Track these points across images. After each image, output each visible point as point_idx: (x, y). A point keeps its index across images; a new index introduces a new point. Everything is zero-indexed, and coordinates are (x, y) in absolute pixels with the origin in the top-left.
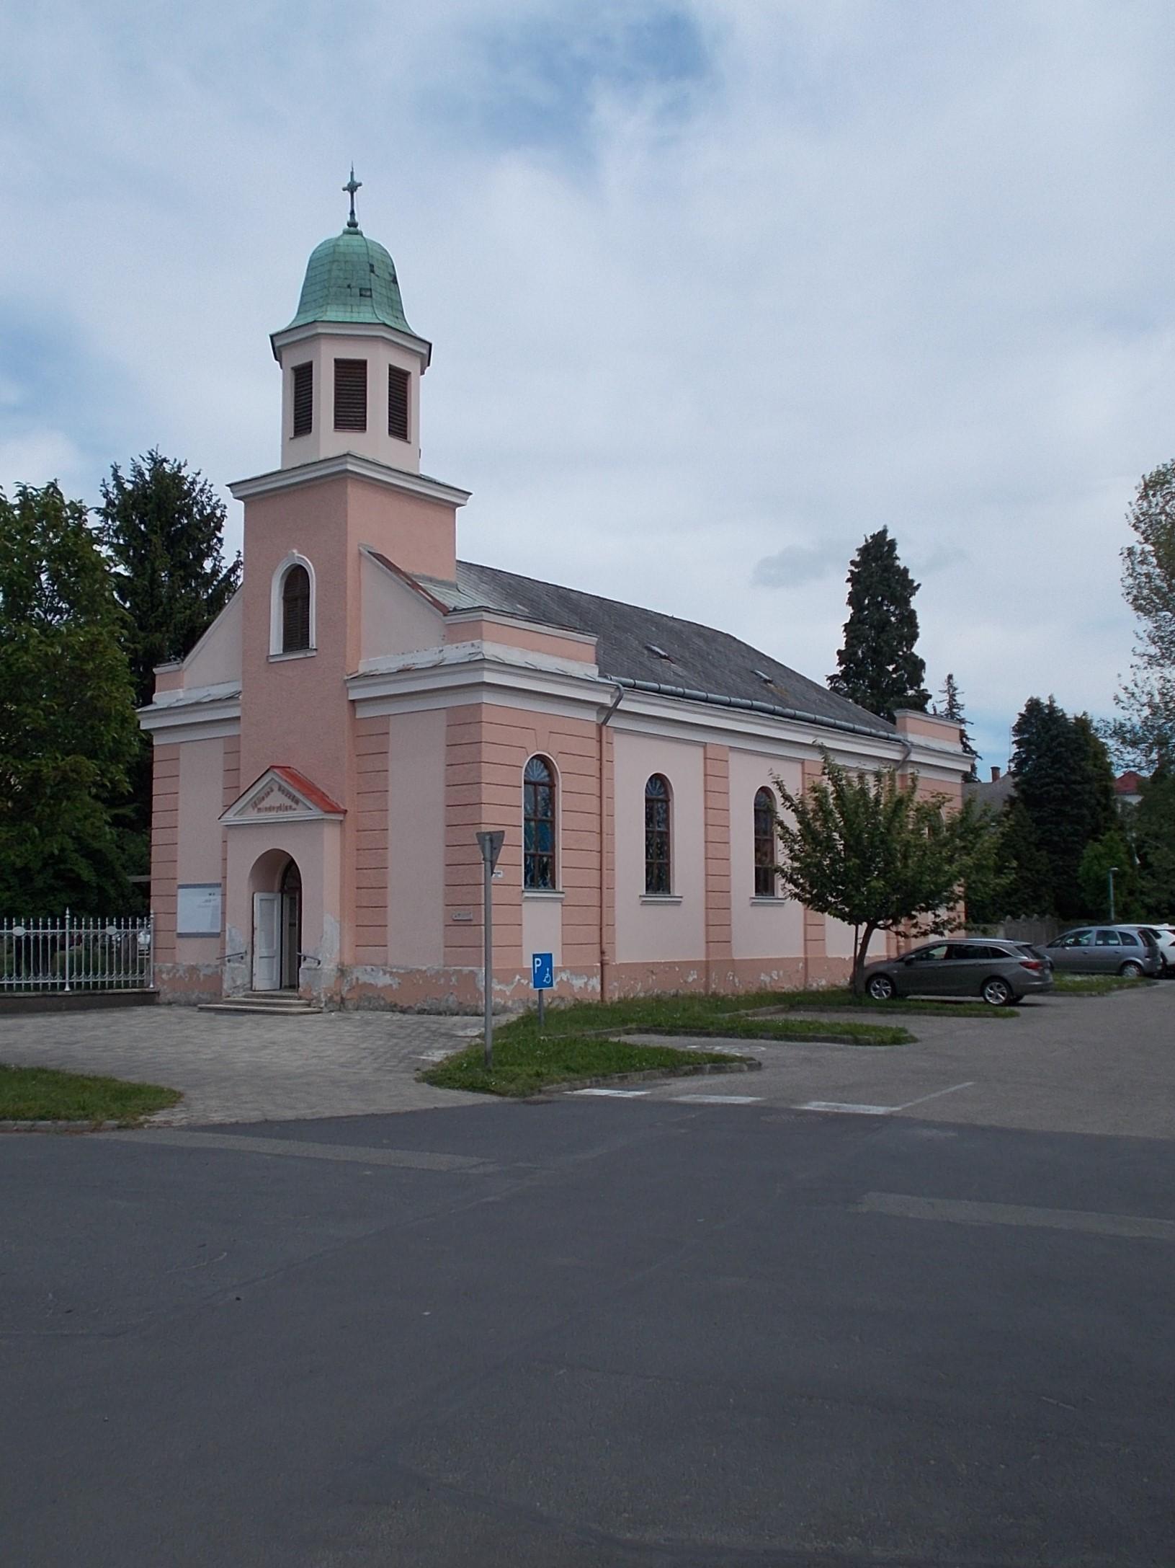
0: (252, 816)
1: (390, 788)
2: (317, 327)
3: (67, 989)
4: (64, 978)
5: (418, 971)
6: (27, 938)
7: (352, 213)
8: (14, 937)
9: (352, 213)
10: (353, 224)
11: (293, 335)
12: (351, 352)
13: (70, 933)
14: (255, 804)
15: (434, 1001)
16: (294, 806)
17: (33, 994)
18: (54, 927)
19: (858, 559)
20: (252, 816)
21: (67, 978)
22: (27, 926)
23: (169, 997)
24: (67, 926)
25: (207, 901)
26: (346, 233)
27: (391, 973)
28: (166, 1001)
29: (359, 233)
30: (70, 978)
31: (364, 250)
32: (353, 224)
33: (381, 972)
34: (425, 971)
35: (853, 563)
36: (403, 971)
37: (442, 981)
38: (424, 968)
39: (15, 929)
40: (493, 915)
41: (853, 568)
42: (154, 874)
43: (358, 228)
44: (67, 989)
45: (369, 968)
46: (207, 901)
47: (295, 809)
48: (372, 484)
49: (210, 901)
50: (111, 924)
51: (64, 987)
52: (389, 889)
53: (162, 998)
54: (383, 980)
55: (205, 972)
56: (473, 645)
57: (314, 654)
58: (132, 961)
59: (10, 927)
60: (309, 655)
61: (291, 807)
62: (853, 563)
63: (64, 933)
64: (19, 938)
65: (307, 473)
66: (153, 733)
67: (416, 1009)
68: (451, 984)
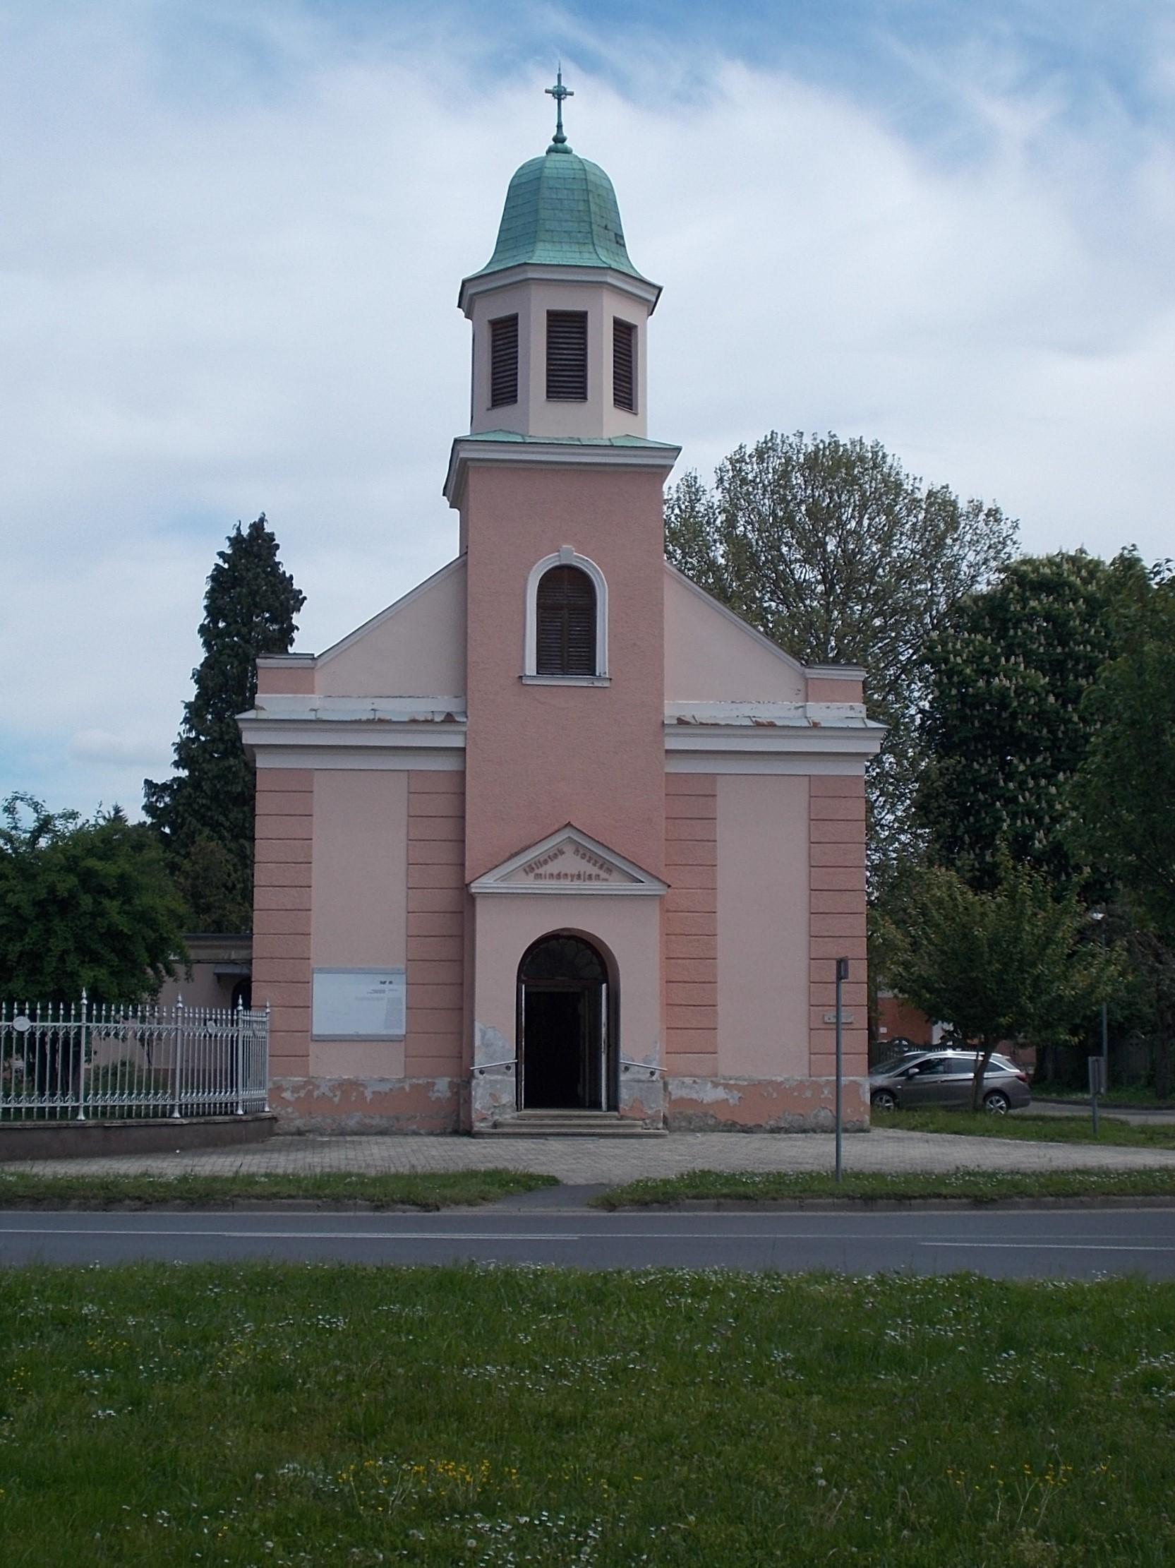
0: (527, 884)
1: (719, 862)
2: (606, 275)
3: (81, 1117)
4: (77, 1100)
5: (770, 1082)
6: (32, 1034)
7: (559, 126)
8: (15, 1033)
9: (559, 126)
10: (559, 139)
11: (646, 291)
12: (568, 302)
13: (88, 1028)
14: (529, 869)
15: (796, 1117)
16: (603, 875)
17: (227, 1118)
18: (67, 1018)
19: (229, 551)
20: (527, 884)
21: (82, 1101)
22: (32, 1017)
23: (299, 1123)
24: (84, 1017)
25: (376, 991)
26: (550, 151)
27: (726, 1086)
28: (294, 1130)
29: (567, 151)
30: (85, 1100)
31: (580, 175)
32: (559, 139)
33: (709, 1085)
34: (782, 1083)
35: (221, 554)
36: (746, 1083)
37: (808, 1094)
38: (780, 1079)
39: (16, 1019)
40: (843, 1014)
41: (220, 562)
42: (260, 945)
43: (566, 143)
44: (81, 1117)
45: (688, 1080)
46: (376, 991)
47: (606, 880)
48: (599, 472)
49: (384, 991)
50: (21, 1013)
51: (77, 1114)
52: (718, 985)
53: (282, 1125)
54: (711, 1094)
55: (377, 1089)
56: (852, 708)
57: (607, 684)
58: (112, 1075)
59: (10, 1018)
60: (596, 684)
61: (598, 876)
62: (221, 554)
63: (80, 1027)
64: (21, 1034)
65: (630, 456)
66: (256, 751)
67: (768, 1127)
68: (823, 1096)
